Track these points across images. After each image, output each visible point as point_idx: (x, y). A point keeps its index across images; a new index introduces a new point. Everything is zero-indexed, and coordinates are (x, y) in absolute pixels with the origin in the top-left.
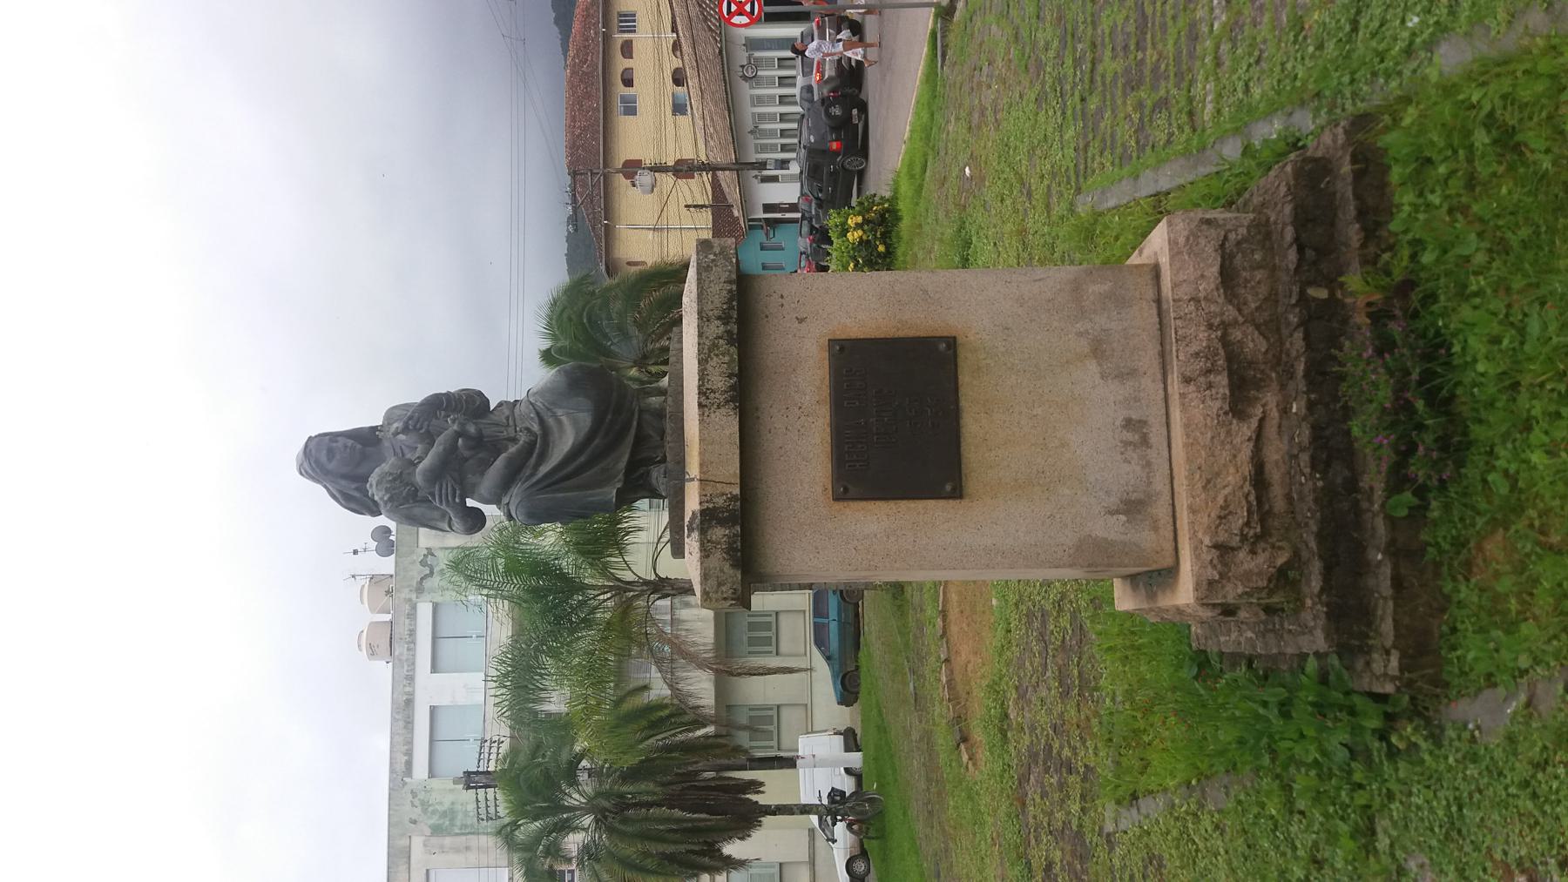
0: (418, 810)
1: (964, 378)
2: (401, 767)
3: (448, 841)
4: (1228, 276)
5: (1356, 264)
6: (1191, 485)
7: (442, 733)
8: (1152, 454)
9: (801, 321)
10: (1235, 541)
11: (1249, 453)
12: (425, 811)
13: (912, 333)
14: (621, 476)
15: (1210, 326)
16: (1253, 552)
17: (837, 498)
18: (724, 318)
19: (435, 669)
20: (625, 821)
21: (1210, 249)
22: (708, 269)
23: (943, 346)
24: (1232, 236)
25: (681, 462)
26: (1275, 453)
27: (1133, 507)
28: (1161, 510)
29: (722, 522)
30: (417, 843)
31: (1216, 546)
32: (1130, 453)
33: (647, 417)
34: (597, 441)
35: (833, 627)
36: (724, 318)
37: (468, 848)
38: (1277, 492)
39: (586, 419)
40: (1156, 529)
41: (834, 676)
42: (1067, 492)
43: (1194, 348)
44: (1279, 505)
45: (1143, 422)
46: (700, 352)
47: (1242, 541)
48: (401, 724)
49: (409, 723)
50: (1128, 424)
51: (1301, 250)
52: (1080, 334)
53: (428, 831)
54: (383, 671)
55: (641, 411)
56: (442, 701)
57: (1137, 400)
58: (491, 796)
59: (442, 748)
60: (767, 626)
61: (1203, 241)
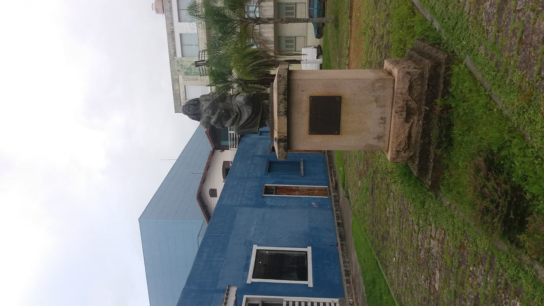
0: (180, 67)
1: (343, 106)
2: (172, 53)
3: (190, 77)
4: (410, 88)
5: (440, 97)
6: (393, 137)
7: (185, 42)
8: (386, 126)
9: (303, 91)
12: (182, 68)
13: (330, 95)
15: (404, 101)
16: (405, 152)
17: (309, 134)
18: (284, 94)
19: (180, 21)
20: (247, 87)
21: (407, 81)
22: (280, 82)
24: (413, 77)
25: (273, 124)
26: (414, 131)
27: (380, 138)
28: (386, 138)
29: (283, 142)
30: (181, 77)
32: (381, 125)
35: (316, 11)
37: (197, 79)
38: (413, 139)
39: (250, 111)
40: (384, 142)
41: (315, 29)
43: (399, 105)
44: (413, 142)
45: (385, 118)
46: (278, 102)
48: (171, 39)
49: (173, 39)
50: (382, 118)
51: (428, 87)
52: (373, 96)
53: (184, 74)
54: (162, 18)
56: (184, 32)
57: (385, 113)
58: (203, 68)
59: (185, 47)
60: (292, 8)
61: (406, 79)
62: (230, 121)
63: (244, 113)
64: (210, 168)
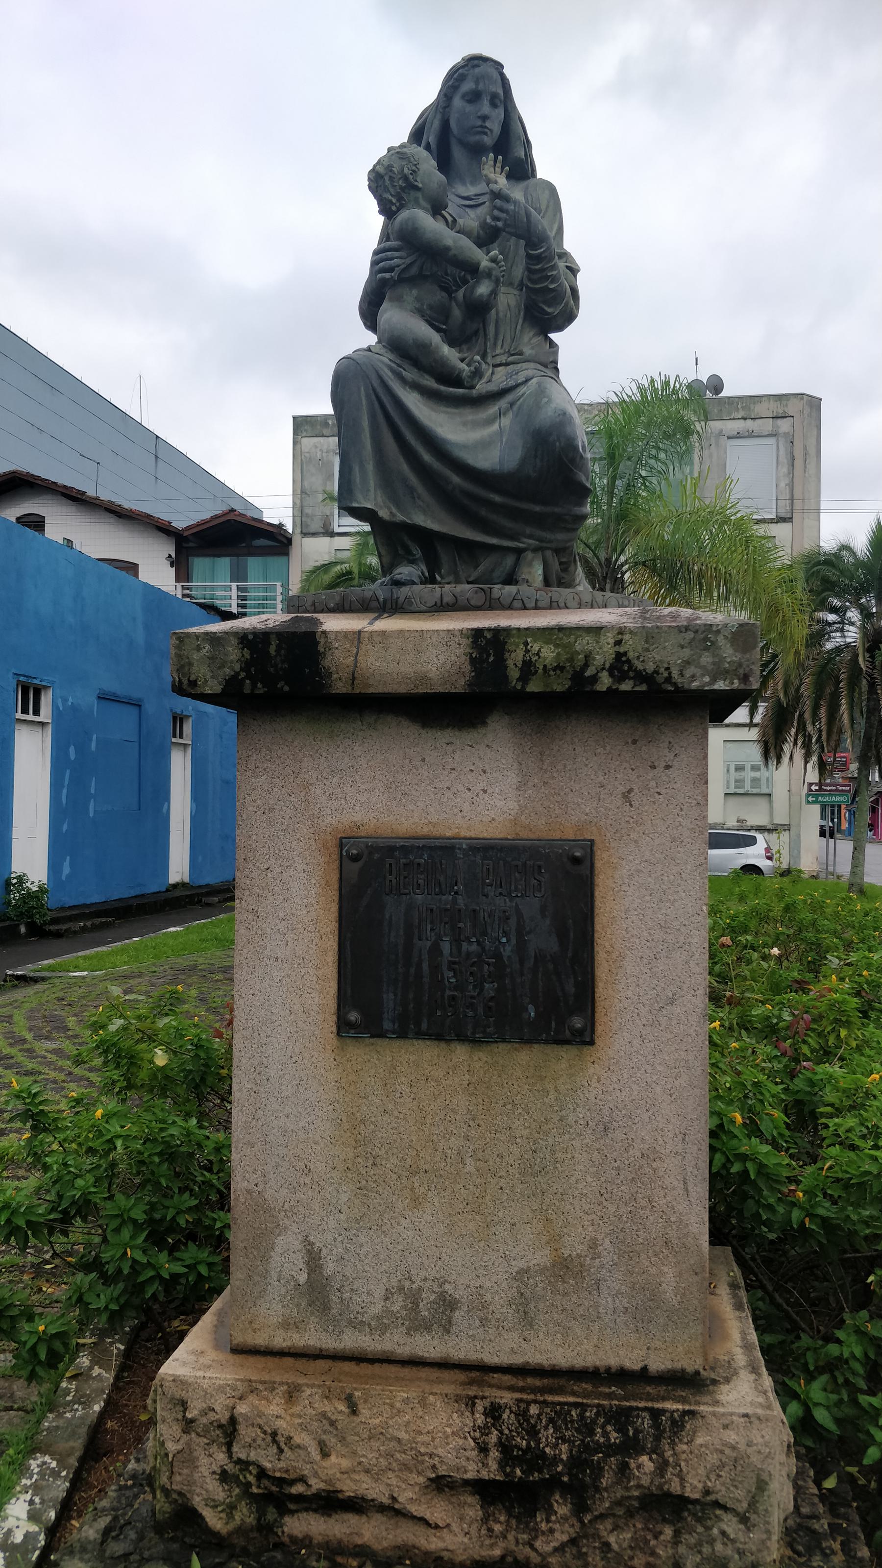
9: (627, 796)
10: (239, 1452)
11: (371, 1495)
13: (602, 972)
14: (400, 517)
18: (621, 665)
23: (578, 1023)
31: (233, 1421)
32: (398, 1304)
33: (509, 561)
34: (456, 479)
36: (621, 665)
39: (487, 460)
40: (286, 1325)
42: (344, 1198)
47: (239, 1461)
50: (448, 1304)
52: (593, 1245)
55: (519, 552)
62: (421, 330)
63: (476, 425)
64: (113, 519)
